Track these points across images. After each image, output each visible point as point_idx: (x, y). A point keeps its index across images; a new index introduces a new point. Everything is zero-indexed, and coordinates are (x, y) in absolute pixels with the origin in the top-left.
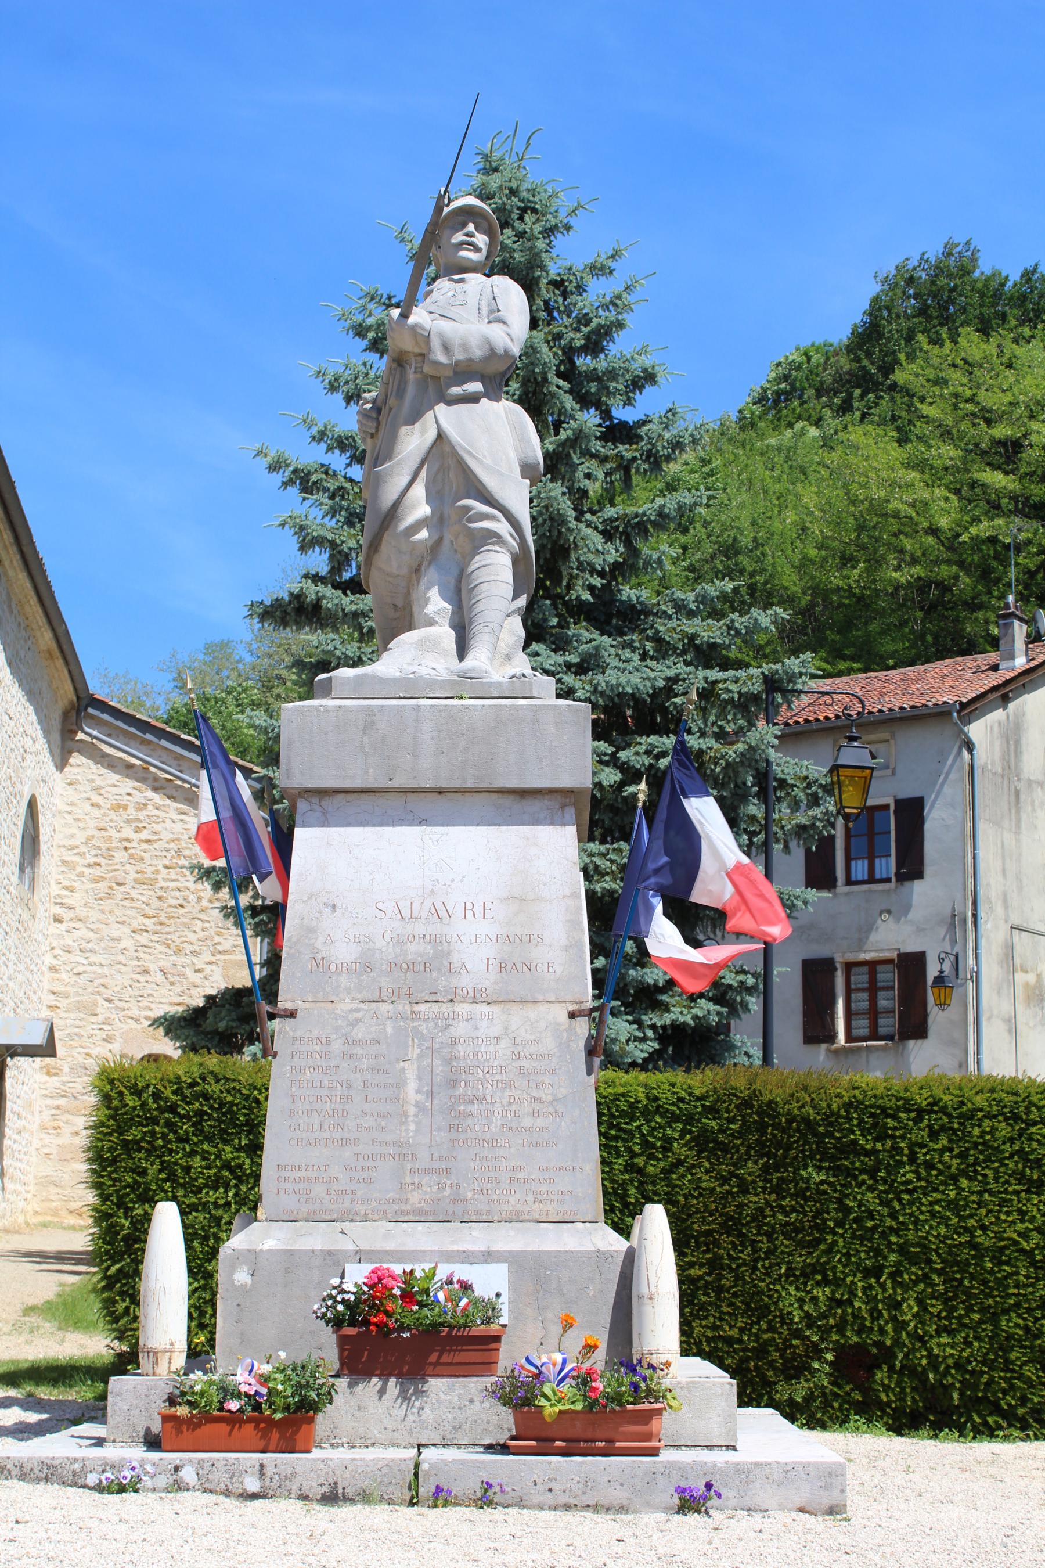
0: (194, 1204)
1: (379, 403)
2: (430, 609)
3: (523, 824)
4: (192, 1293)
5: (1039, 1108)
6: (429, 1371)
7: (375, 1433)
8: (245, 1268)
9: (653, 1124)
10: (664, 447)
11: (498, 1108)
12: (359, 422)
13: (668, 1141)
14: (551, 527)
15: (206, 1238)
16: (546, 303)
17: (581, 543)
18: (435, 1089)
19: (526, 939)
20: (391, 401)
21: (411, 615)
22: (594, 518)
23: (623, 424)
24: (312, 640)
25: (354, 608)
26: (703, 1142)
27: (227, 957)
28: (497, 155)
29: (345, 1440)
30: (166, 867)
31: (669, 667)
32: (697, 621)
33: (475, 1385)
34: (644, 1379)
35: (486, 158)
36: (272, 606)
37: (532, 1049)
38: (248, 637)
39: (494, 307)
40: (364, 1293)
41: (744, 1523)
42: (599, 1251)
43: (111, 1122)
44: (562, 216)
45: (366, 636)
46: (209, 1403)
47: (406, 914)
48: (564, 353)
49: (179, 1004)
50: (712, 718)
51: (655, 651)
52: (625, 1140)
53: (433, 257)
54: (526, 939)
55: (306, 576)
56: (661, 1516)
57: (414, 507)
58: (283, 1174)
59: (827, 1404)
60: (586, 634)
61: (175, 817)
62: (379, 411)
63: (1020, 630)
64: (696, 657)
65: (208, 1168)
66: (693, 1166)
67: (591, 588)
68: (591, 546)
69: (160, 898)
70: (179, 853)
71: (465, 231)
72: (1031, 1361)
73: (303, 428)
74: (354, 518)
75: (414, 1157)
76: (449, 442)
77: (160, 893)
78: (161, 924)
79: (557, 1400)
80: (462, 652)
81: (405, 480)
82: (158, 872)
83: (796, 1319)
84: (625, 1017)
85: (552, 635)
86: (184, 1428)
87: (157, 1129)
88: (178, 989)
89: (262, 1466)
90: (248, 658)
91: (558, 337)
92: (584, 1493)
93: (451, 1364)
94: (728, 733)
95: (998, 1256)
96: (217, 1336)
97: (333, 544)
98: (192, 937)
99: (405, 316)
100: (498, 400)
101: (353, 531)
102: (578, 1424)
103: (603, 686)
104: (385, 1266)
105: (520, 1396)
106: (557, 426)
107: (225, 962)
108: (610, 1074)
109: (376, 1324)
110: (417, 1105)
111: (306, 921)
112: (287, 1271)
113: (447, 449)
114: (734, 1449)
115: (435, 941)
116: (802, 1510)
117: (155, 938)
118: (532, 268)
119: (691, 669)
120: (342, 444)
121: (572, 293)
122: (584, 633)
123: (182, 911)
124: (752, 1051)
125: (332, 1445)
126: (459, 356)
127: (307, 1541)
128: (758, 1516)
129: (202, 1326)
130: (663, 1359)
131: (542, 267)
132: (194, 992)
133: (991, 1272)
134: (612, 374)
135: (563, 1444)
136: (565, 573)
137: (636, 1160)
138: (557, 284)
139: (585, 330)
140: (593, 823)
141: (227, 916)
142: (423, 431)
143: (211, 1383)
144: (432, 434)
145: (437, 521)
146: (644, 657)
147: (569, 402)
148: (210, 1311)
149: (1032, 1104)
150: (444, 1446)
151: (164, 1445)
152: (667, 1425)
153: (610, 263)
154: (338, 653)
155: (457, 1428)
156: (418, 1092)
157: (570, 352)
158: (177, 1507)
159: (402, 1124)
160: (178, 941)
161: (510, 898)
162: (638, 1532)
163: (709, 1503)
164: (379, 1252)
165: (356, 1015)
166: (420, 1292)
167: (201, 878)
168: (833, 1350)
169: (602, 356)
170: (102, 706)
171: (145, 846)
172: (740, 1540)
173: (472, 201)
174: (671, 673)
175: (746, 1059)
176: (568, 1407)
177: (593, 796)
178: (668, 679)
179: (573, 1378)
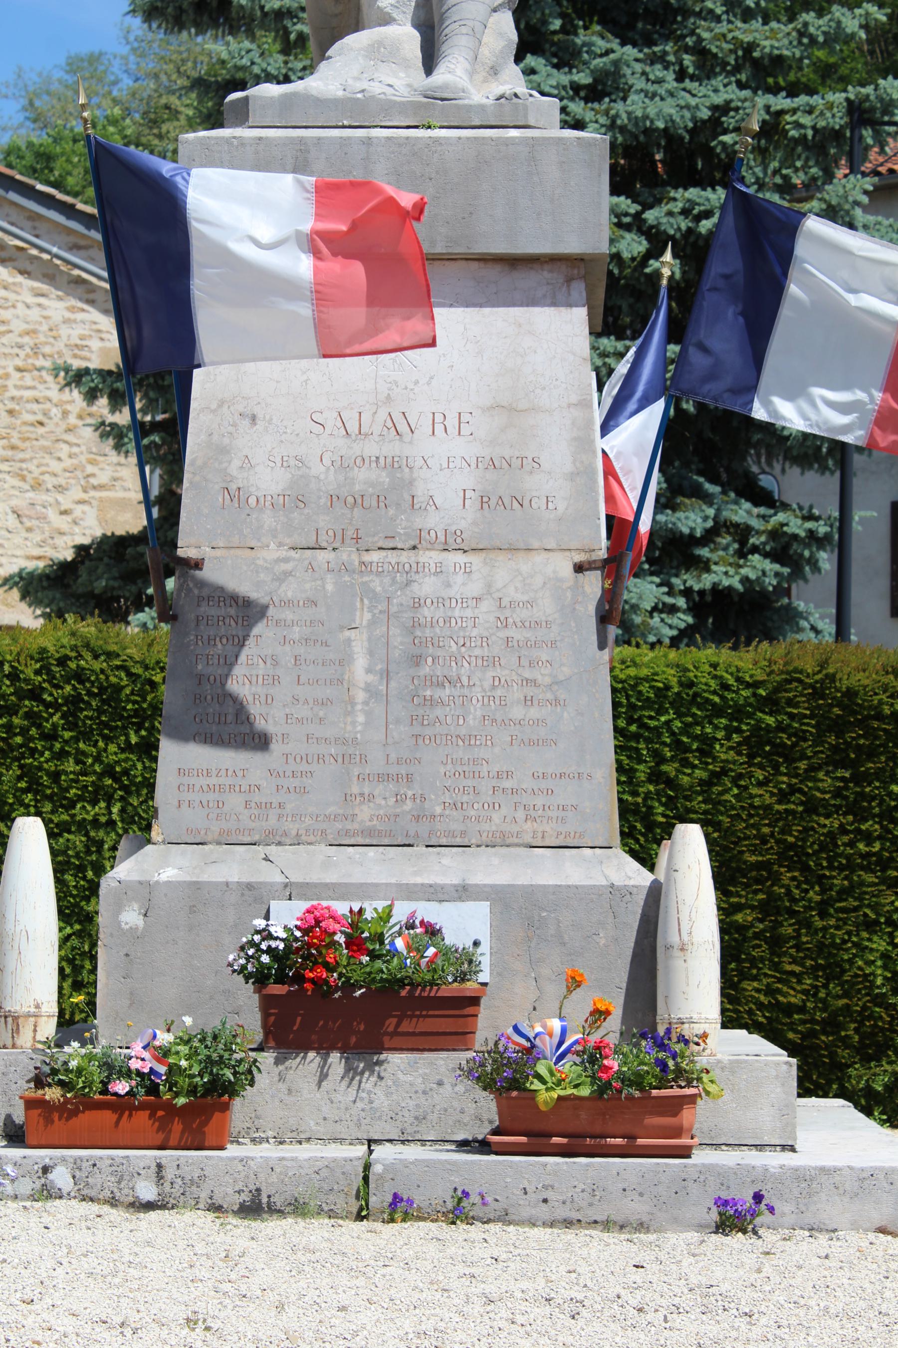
0: (65, 823)
3: (514, 305)
4: (64, 941)
7: (312, 1125)
8: (136, 906)
11: (477, 693)
13: (707, 742)
15: (81, 869)
19: (516, 463)
26: (756, 744)
27: (104, 494)
29: (270, 1133)
30: (19, 370)
31: (716, 91)
32: (757, 24)
33: (445, 1063)
34: (674, 1056)
37: (523, 614)
40: (296, 939)
41: (804, 1246)
42: (612, 886)
45: (293, 46)
46: (89, 1084)
47: (353, 428)
49: (39, 558)
50: (775, 164)
51: (697, 67)
52: (648, 741)
54: (516, 463)
56: (693, 1236)
58: (186, 780)
61: (31, 300)
64: (754, 76)
65: (85, 774)
66: (740, 776)
69: (11, 412)
70: (36, 350)
75: (364, 759)
77: (11, 405)
78: (13, 448)
79: (557, 1082)
80: (429, 63)
83: (879, 981)
84: (650, 579)
85: (553, 44)
86: (56, 1116)
87: (16, 721)
88: (37, 537)
89: (159, 1166)
90: (127, 82)
92: (591, 1205)
93: (413, 1034)
94: (795, 186)
96: (99, 1000)
98: (55, 466)
102: (583, 1115)
103: (623, 119)
104: (325, 903)
105: (507, 1077)
107: (101, 500)
108: (628, 651)
109: (312, 981)
110: (368, 688)
111: (215, 438)
112: (192, 910)
114: (792, 1149)
115: (393, 465)
116: (882, 1230)
119: (746, 93)
123: (41, 430)
124: (820, 625)
125: (253, 1140)
127: (221, 1264)
128: (823, 1238)
129: (78, 986)
130: (699, 1029)
132: (60, 541)
135: (564, 1141)
137: (665, 768)
140: (610, 310)
141: (104, 436)
143: (90, 1057)
146: (681, 75)
148: (88, 965)
150: (403, 1142)
151: (29, 1139)
152: (702, 1117)
154: (256, 70)
155: (420, 1119)
156: (369, 671)
158: (47, 1219)
159: (347, 713)
160: (36, 472)
161: (495, 407)
162: (662, 1256)
163: (758, 1221)
164: (315, 885)
166: (371, 939)
172: (800, 1267)
174: (718, 100)
175: (812, 635)
176: (569, 1091)
177: (610, 273)
178: (714, 108)
179: (577, 1053)
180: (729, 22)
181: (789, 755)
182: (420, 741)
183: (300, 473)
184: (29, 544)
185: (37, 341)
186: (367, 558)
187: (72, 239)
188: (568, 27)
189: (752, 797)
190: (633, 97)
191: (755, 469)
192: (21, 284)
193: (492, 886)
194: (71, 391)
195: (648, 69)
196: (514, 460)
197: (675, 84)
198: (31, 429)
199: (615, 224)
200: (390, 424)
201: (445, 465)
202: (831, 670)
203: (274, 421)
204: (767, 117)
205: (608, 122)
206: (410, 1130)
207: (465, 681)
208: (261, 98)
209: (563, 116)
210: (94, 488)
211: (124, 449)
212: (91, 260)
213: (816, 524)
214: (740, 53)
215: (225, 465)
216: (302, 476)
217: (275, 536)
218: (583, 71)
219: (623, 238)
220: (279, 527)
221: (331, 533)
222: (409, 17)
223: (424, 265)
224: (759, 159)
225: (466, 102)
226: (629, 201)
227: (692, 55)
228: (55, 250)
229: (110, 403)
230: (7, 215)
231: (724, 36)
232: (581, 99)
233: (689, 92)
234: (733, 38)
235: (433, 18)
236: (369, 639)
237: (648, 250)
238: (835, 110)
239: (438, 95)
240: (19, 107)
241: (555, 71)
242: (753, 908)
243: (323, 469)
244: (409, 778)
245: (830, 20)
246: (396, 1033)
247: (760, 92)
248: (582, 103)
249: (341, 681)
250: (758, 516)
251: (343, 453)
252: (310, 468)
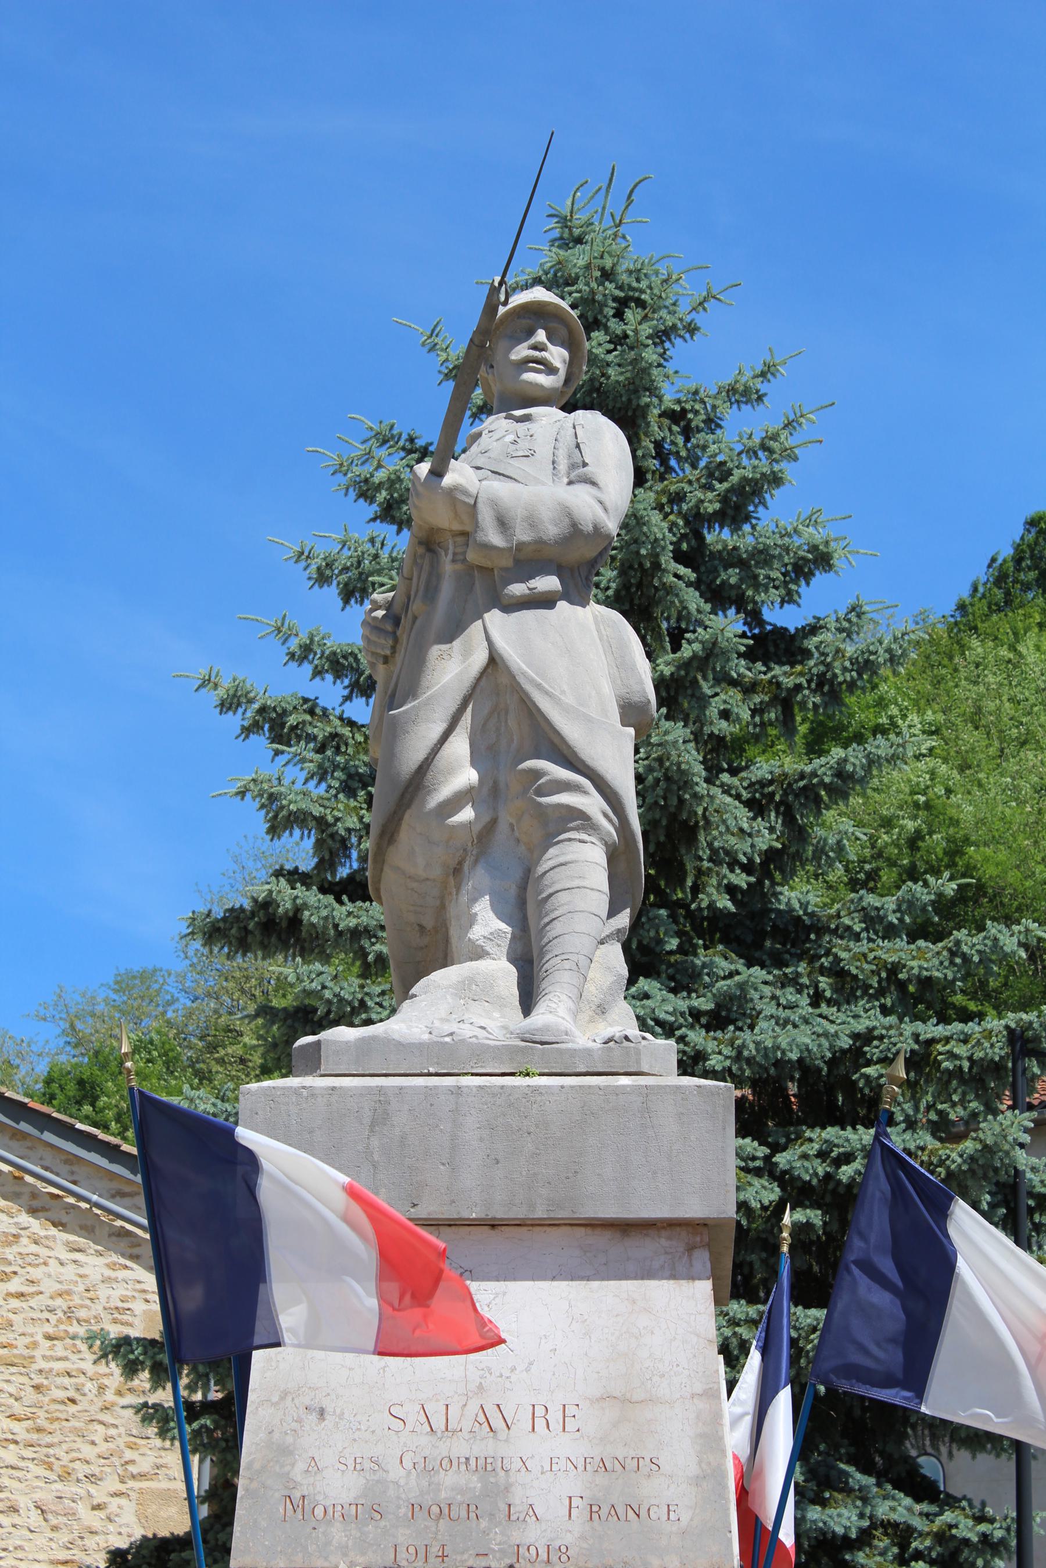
1: (397, 608)
2: (477, 933)
3: (627, 1278)
10: (845, 669)
12: (365, 637)
14: (667, 790)
16: (658, 445)
17: (715, 819)
19: (631, 1464)
20: (416, 606)
21: (447, 940)
22: (735, 781)
23: (780, 632)
24: (289, 973)
25: (353, 922)
27: (145, 1484)
28: (580, 217)
30: (49, 1337)
31: (856, 1017)
32: (901, 943)
35: (564, 222)
36: (224, 919)
38: (181, 966)
39: (579, 460)
44: (683, 309)
47: (438, 1423)
48: (687, 523)
53: (480, 383)
54: (631, 1464)
55: (278, 873)
60: (724, 964)
61: (65, 1256)
62: (397, 621)
67: (731, 890)
68: (731, 823)
69: (37, 1388)
70: (69, 1314)
71: (532, 341)
73: (276, 641)
74: (356, 783)
76: (507, 669)
77: (38, 1380)
78: (39, 1430)
80: (528, 1001)
81: (437, 729)
82: (35, 1345)
85: (670, 965)
88: (64, 1537)
91: (678, 498)
97: (321, 822)
98: (88, 1452)
99: (437, 473)
100: (584, 604)
101: (353, 803)
106: (676, 639)
107: (141, 1492)
111: (276, 1436)
113: (504, 680)
115: (485, 1467)
117: (28, 1453)
118: (636, 391)
119: (892, 1019)
120: (338, 665)
121: (699, 430)
122: (719, 962)
123: (72, 1409)
126: (523, 535)
131: (653, 390)
132: (90, 1542)
134: (763, 556)
136: (689, 866)
138: (676, 417)
139: (721, 487)
141: (146, 1420)
142: (467, 653)
144: (480, 658)
145: (488, 793)
146: (816, 999)
147: (693, 600)
154: (327, 994)
157: (696, 521)
160: (66, 1459)
167: (105, 1356)
169: (747, 528)
171: (15, 1303)
173: (539, 294)
174: (860, 1026)
178: (855, 1036)
180: (870, 940)
183: (376, 1478)
184: (54, 1545)
185: (71, 1304)
187: (115, 1185)
188: (687, 946)
190: (762, 1024)
191: (913, 1453)
192: (54, 1237)
194: (107, 1364)
195: (778, 993)
196: (628, 1461)
197: (810, 1010)
198: (62, 1407)
199: (742, 1169)
200: (481, 1418)
201: (547, 1467)
203: (346, 1416)
204: (916, 1047)
205: (734, 1054)
208: (335, 1042)
209: (681, 1046)
210: (133, 1477)
211: (169, 1434)
212: (135, 1208)
213: (990, 1527)
214: (884, 975)
215: (287, 1468)
216: (378, 1481)
217: (345, 1555)
218: (704, 996)
219: (750, 1184)
220: (350, 1543)
221: (412, 1550)
222: (505, 950)
224: (909, 1094)
225: (570, 1045)
226: (756, 1144)
227: (828, 977)
228: (95, 1198)
229: (151, 1379)
230: (41, 1159)
231: (865, 955)
232: (702, 1026)
233: (826, 1018)
234: (875, 958)
235: (531, 951)
237: (781, 1198)
238: (994, 1039)
239: (537, 1038)
240: (59, 1031)
241: (672, 996)
245: (985, 938)
247: (907, 1019)
248: (703, 1032)
250: (921, 1514)
251: (426, 1453)
252: (387, 1472)
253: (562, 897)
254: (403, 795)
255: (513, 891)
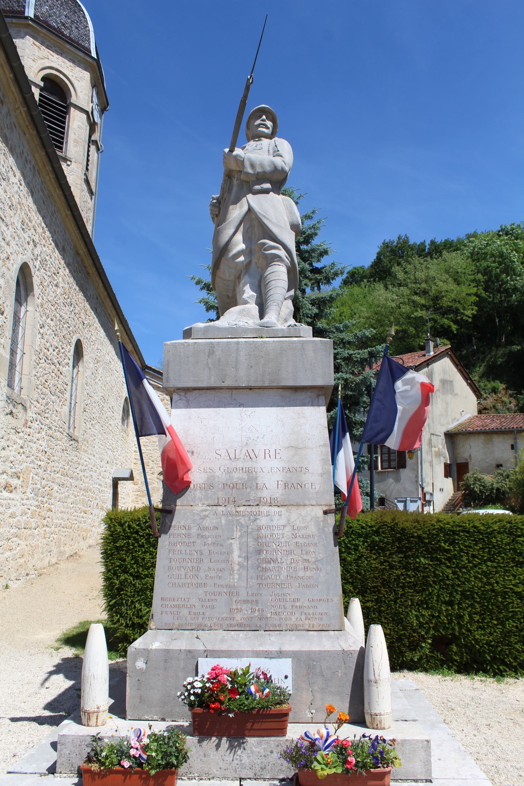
2: (245, 296)
3: (296, 406)
5: (521, 529)
6: (246, 732)
7: (214, 771)
8: (142, 659)
9: (350, 539)
13: (357, 546)
18: (249, 555)
26: (372, 547)
29: (196, 775)
32: (344, 334)
37: (303, 532)
42: (344, 650)
43: (110, 538)
47: (232, 456)
57: (236, 245)
58: (165, 603)
59: (428, 661)
63: (431, 344)
66: (368, 557)
72: (519, 641)
75: (238, 594)
80: (262, 315)
81: (232, 231)
83: (415, 625)
86: (97, 777)
95: (504, 595)
110: (239, 564)
112: (166, 661)
113: (253, 216)
115: (249, 471)
119: (343, 350)
125: (189, 778)
126: (259, 170)
133: (502, 602)
134: (313, 250)
142: (241, 207)
144: (245, 208)
145: (248, 252)
149: (518, 528)
150: (255, 779)
153: (311, 215)
159: (231, 575)
164: (218, 651)
165: (205, 513)
168: (431, 638)
170: (150, 368)
181: (383, 550)
182: (261, 586)
186: (239, 509)
189: (372, 564)
193: (293, 651)
202: (397, 521)
206: (258, 774)
207: (279, 560)
217: (201, 501)
223: (89, 146)
236: (240, 543)
242: (372, 601)
243: (220, 473)
244: (257, 602)
246: (251, 729)
249: (228, 561)
253: (273, 282)
254: (221, 252)
255: (257, 283)
